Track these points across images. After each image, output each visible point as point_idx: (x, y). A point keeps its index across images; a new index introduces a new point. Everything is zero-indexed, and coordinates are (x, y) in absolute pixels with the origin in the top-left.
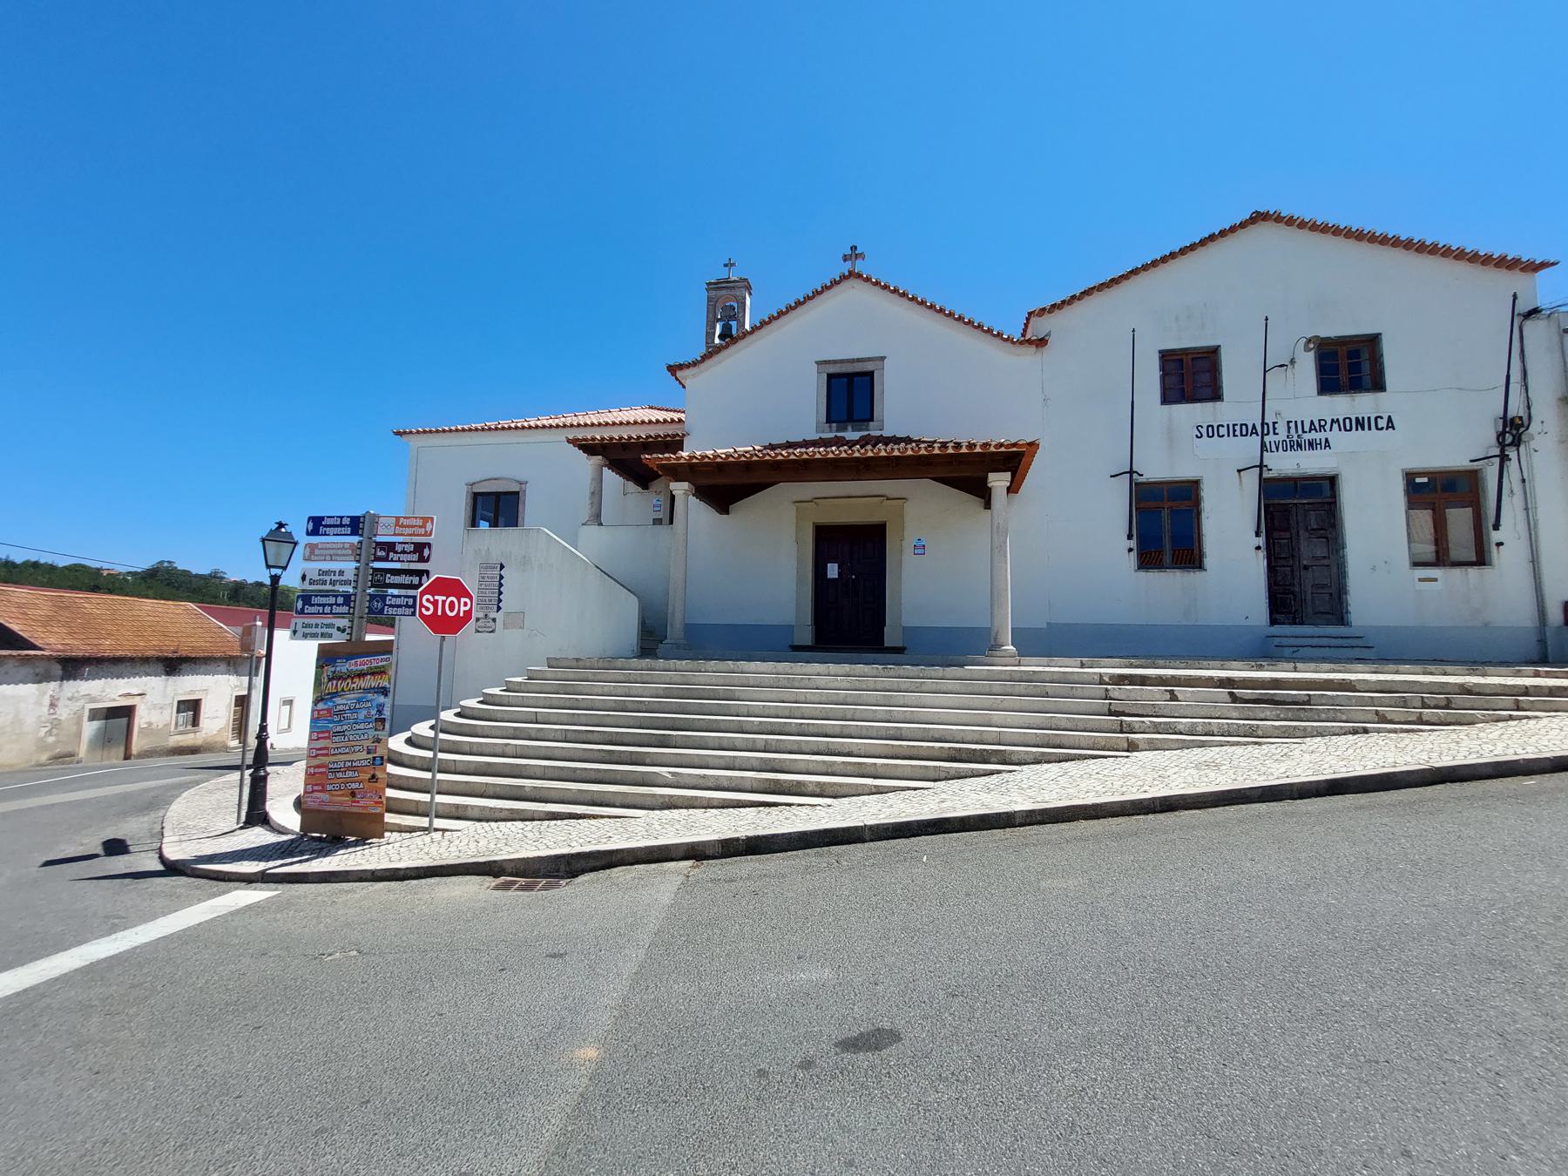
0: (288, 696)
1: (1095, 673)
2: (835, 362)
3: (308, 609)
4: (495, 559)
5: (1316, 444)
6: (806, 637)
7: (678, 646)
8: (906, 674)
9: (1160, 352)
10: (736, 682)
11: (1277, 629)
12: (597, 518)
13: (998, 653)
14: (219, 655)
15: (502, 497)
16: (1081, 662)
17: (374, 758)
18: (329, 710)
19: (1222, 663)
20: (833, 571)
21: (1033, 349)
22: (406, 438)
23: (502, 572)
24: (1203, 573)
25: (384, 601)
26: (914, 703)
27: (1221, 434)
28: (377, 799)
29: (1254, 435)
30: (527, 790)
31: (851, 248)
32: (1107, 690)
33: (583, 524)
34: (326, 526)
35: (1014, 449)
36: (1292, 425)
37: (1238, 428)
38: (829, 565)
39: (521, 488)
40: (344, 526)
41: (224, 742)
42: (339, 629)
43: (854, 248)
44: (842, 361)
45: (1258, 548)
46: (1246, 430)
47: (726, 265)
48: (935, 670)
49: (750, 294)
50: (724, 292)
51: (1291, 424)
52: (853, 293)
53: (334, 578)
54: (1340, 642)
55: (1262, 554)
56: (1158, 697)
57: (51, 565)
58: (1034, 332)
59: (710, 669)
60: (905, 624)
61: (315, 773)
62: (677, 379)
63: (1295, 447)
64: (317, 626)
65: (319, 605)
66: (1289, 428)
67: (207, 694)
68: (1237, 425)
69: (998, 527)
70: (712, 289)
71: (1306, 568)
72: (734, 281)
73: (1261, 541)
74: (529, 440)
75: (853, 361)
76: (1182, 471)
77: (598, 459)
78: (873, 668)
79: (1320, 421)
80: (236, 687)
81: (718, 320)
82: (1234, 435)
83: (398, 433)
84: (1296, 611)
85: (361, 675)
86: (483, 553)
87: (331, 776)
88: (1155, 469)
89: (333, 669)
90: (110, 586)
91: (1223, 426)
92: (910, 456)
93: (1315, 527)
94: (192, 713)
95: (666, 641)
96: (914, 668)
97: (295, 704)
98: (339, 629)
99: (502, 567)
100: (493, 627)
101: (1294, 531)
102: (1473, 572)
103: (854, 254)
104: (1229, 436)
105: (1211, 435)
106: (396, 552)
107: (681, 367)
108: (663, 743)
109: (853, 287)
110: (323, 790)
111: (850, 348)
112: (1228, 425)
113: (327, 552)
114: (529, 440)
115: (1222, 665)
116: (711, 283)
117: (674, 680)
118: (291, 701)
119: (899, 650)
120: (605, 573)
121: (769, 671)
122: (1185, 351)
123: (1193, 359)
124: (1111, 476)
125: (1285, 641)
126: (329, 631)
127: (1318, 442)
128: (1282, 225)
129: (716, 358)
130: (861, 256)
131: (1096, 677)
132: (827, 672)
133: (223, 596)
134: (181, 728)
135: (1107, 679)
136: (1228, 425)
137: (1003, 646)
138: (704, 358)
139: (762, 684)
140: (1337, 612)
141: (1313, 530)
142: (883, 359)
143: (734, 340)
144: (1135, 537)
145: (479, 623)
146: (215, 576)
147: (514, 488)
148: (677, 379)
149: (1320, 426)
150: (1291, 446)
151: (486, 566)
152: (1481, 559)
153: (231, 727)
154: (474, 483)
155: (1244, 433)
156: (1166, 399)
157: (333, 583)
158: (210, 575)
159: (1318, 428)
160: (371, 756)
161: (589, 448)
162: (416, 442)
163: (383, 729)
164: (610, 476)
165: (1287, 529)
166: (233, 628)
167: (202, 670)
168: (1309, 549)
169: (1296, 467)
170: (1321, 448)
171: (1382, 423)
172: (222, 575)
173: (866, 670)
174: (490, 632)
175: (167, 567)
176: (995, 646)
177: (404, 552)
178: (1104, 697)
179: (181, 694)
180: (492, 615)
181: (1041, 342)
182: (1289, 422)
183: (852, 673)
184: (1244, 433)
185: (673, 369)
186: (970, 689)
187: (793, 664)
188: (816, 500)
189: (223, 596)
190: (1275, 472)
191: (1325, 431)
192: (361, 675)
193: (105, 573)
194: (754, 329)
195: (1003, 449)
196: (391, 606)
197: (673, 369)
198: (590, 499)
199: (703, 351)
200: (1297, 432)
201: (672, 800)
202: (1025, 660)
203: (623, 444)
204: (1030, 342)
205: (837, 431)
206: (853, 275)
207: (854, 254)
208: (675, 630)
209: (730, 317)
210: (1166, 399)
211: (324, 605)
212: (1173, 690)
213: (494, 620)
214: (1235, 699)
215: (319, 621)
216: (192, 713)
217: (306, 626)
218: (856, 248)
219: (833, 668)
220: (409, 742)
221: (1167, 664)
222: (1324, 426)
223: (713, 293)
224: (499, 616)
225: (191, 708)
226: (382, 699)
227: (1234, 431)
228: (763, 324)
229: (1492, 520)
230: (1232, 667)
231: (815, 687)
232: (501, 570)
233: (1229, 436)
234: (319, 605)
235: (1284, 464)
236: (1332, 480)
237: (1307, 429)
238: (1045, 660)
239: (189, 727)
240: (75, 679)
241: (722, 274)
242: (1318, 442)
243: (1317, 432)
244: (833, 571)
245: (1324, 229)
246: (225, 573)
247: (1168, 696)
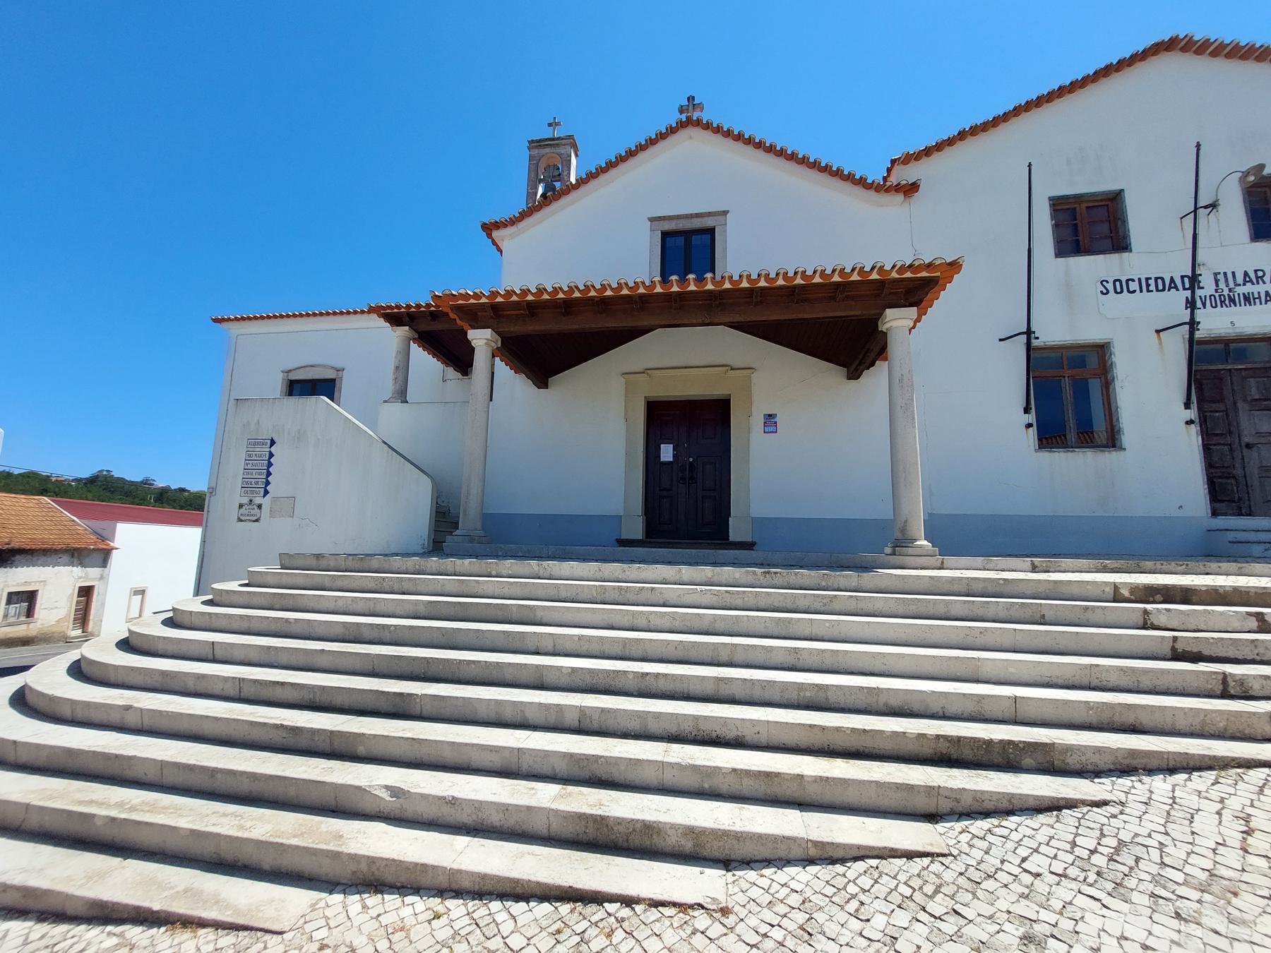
0: (139, 585)
1: (1106, 583)
4: (265, 435)
5: (1254, 299)
6: (636, 530)
7: (471, 539)
8: (800, 581)
9: (1051, 199)
10: (540, 593)
11: (1221, 522)
12: (401, 395)
13: (910, 551)
14: (60, 547)
16: (1033, 564)
19: (1239, 565)
20: (667, 453)
21: (900, 197)
22: (225, 325)
23: (273, 449)
24: (1122, 453)
26: (827, 634)
27: (1131, 290)
29: (1173, 290)
30: (99, 823)
31: (688, 99)
32: (1146, 612)
33: (385, 402)
35: (924, 274)
36: (1221, 277)
37: (1152, 282)
38: (662, 445)
41: (63, 632)
43: (691, 99)
44: (679, 217)
47: (550, 125)
48: (846, 576)
49: (577, 155)
50: (547, 150)
51: (1219, 277)
52: (692, 144)
55: (1194, 429)
56: (1236, 624)
57: (8, 472)
58: (904, 175)
59: (504, 572)
62: (494, 243)
63: (1227, 302)
66: (1217, 282)
67: (44, 585)
68: (1150, 278)
69: (901, 380)
70: (537, 147)
71: (1249, 446)
72: (558, 139)
73: (1192, 414)
75: (691, 216)
76: (1089, 333)
77: (404, 331)
78: (747, 571)
79: (1256, 271)
80: (80, 578)
81: (540, 181)
82: (1148, 291)
83: (216, 320)
84: (1240, 499)
88: (1052, 332)
90: (57, 490)
91: (1133, 280)
92: (781, 287)
93: (1257, 397)
94: (27, 604)
95: (457, 532)
96: (813, 573)
97: (148, 594)
99: (273, 443)
100: (259, 516)
101: (1229, 403)
104: (1141, 291)
105: (1119, 290)
107: (498, 225)
108: (399, 709)
109: (691, 138)
112: (1140, 279)
115: (1240, 568)
116: (532, 141)
117: (448, 589)
118: (144, 591)
119: (749, 546)
120: (393, 450)
121: (591, 575)
122: (1079, 198)
123: (1088, 208)
124: (1000, 340)
125: (1252, 536)
127: (1256, 296)
129: (537, 216)
131: (1107, 589)
132: (677, 578)
133: (150, 499)
134: (12, 620)
135: (1126, 593)
136: (1140, 279)
137: (916, 540)
138: (523, 215)
139: (580, 598)
141: (1256, 400)
142: (725, 213)
143: (558, 195)
144: (1033, 410)
145: (242, 511)
146: (146, 482)
147: (330, 375)
148: (494, 243)
149: (1257, 278)
150: (1221, 302)
151: (254, 442)
153: (72, 617)
154: (290, 371)
155: (1160, 287)
156: (1059, 254)
158: (142, 482)
159: (1255, 281)
161: (395, 317)
162: (235, 329)
164: (418, 353)
165: (1222, 400)
166: (82, 520)
167: (39, 562)
169: (1230, 325)
170: (1261, 304)
172: (152, 482)
173: (737, 576)
174: (254, 521)
175: (105, 475)
176: (901, 543)
178: (1141, 622)
179: (14, 586)
180: (258, 500)
181: (910, 189)
182: (1216, 274)
183: (716, 579)
184: (1160, 287)
185: (488, 228)
186: (912, 609)
187: (625, 566)
188: (648, 371)
189: (150, 499)
190: (1205, 332)
191: (1264, 283)
193: (54, 479)
194: (581, 182)
195: (908, 275)
197: (488, 228)
198: (394, 374)
199: (523, 206)
200: (1227, 285)
201: (374, 868)
202: (950, 560)
203: (432, 313)
204: (898, 188)
208: (469, 520)
209: (554, 177)
210: (1059, 254)
212: (1261, 614)
213: (260, 506)
216: (27, 604)
218: (693, 98)
219: (686, 571)
220: (79, 671)
221: (1159, 566)
222: (1262, 277)
223: (536, 152)
224: (266, 502)
225: (27, 599)
227: (1148, 285)
228: (591, 176)
230: (1256, 572)
231: (661, 602)
232: (271, 447)
233: (1141, 291)
235: (1215, 322)
237: (1240, 279)
238: (979, 561)
239: (23, 618)
240: (34, 566)
241: (547, 133)
242: (1256, 296)
243: (1253, 284)
244: (667, 453)
246: (154, 481)
247: (1254, 624)
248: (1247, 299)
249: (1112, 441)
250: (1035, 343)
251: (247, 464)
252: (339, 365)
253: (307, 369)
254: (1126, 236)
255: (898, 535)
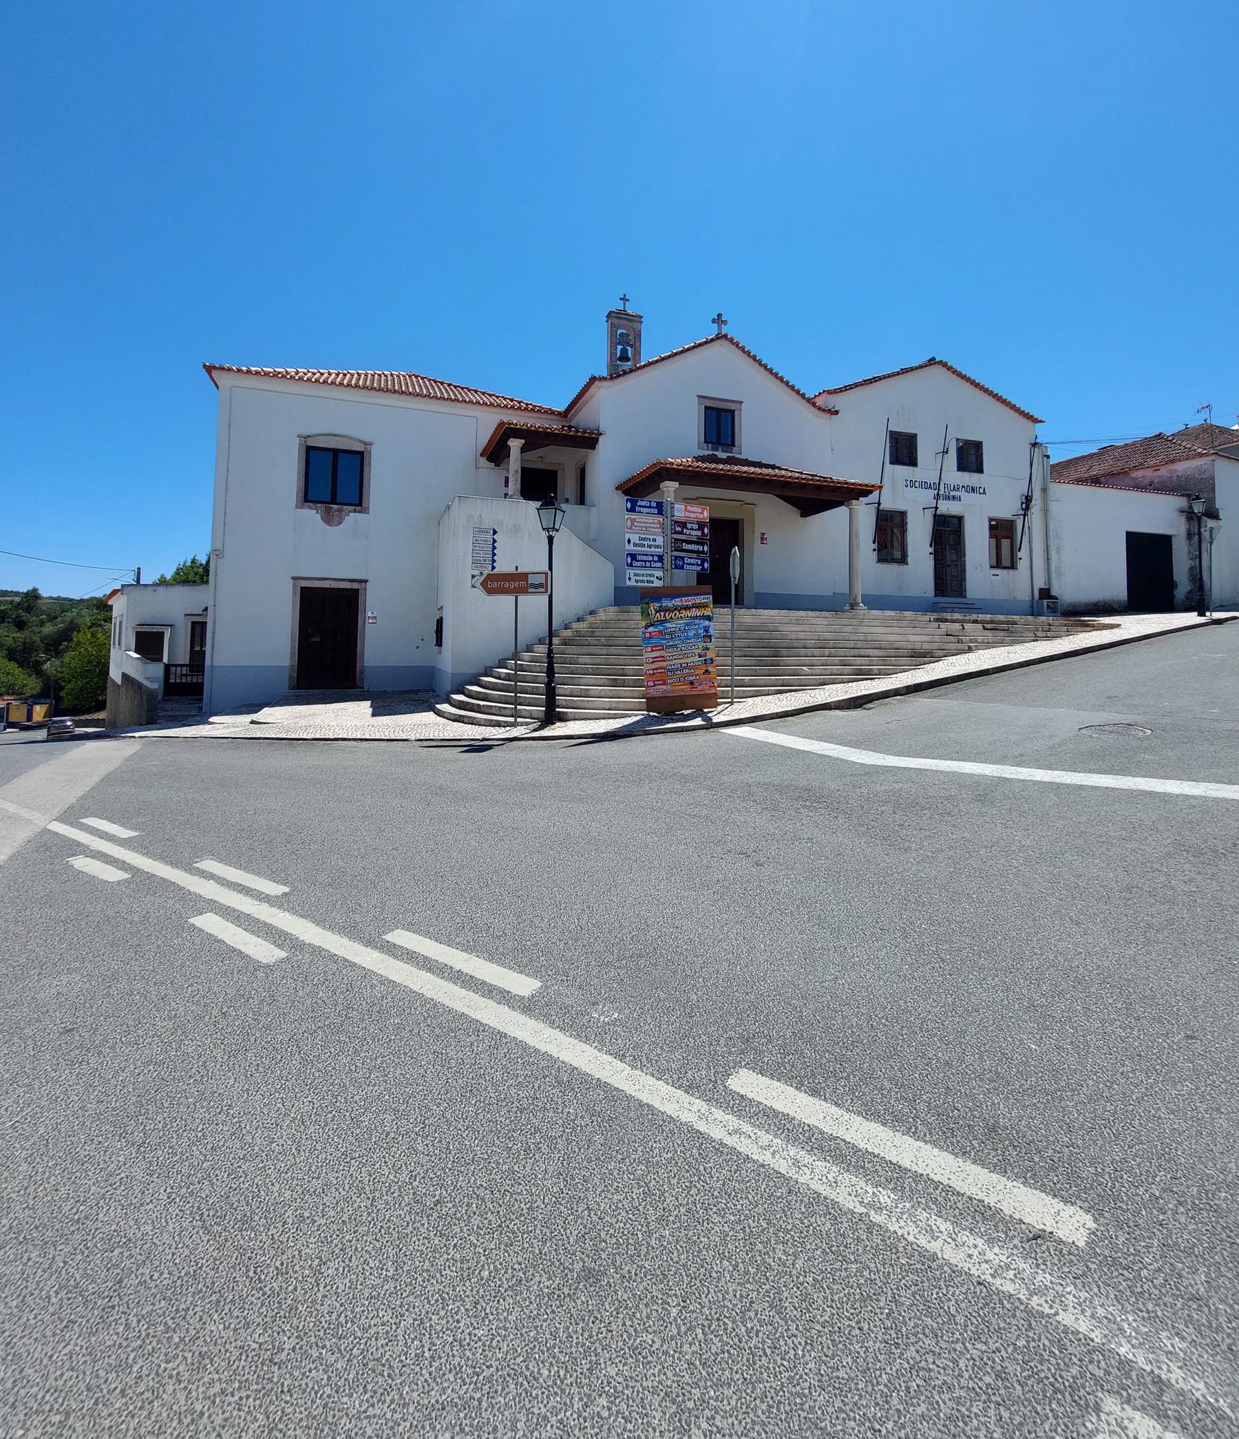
2: (711, 398)
3: (635, 564)
4: (487, 524)
13: (858, 608)
15: (340, 455)
17: (705, 660)
18: (660, 632)
25: (683, 561)
28: (711, 685)
34: (640, 506)
39: (366, 448)
40: (653, 507)
42: (657, 578)
45: (931, 554)
46: (926, 486)
52: (721, 348)
53: (650, 543)
54: (966, 606)
55: (932, 556)
60: (756, 590)
61: (654, 674)
64: (643, 575)
65: (642, 561)
71: (949, 566)
73: (931, 550)
74: (368, 400)
75: (722, 400)
76: (900, 507)
85: (687, 608)
86: (476, 519)
87: (669, 674)
89: (659, 605)
98: (657, 578)
99: (495, 532)
102: (1011, 571)
103: (719, 320)
106: (687, 529)
110: (665, 683)
111: (721, 391)
113: (643, 525)
114: (368, 400)
125: (816, 651)
126: (652, 579)
128: (945, 369)
130: (725, 322)
140: (960, 591)
152: (1013, 566)
154: (309, 436)
157: (650, 547)
160: (703, 659)
163: (711, 641)
165: (941, 544)
168: (950, 556)
171: (982, 491)
177: (692, 529)
192: (687, 608)
196: (688, 564)
205: (713, 450)
206: (720, 337)
207: (719, 320)
211: (645, 561)
214: (985, 628)
215: (645, 572)
217: (636, 575)
226: (707, 623)
229: (1018, 547)
234: (642, 561)
235: (946, 507)
236: (960, 519)
245: (963, 377)
248: (954, 497)
249: (903, 560)
250: (881, 508)
251: (475, 546)
252: (366, 438)
253: (329, 437)
254: (916, 459)
255: (852, 601)
